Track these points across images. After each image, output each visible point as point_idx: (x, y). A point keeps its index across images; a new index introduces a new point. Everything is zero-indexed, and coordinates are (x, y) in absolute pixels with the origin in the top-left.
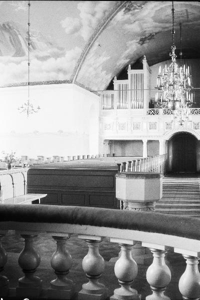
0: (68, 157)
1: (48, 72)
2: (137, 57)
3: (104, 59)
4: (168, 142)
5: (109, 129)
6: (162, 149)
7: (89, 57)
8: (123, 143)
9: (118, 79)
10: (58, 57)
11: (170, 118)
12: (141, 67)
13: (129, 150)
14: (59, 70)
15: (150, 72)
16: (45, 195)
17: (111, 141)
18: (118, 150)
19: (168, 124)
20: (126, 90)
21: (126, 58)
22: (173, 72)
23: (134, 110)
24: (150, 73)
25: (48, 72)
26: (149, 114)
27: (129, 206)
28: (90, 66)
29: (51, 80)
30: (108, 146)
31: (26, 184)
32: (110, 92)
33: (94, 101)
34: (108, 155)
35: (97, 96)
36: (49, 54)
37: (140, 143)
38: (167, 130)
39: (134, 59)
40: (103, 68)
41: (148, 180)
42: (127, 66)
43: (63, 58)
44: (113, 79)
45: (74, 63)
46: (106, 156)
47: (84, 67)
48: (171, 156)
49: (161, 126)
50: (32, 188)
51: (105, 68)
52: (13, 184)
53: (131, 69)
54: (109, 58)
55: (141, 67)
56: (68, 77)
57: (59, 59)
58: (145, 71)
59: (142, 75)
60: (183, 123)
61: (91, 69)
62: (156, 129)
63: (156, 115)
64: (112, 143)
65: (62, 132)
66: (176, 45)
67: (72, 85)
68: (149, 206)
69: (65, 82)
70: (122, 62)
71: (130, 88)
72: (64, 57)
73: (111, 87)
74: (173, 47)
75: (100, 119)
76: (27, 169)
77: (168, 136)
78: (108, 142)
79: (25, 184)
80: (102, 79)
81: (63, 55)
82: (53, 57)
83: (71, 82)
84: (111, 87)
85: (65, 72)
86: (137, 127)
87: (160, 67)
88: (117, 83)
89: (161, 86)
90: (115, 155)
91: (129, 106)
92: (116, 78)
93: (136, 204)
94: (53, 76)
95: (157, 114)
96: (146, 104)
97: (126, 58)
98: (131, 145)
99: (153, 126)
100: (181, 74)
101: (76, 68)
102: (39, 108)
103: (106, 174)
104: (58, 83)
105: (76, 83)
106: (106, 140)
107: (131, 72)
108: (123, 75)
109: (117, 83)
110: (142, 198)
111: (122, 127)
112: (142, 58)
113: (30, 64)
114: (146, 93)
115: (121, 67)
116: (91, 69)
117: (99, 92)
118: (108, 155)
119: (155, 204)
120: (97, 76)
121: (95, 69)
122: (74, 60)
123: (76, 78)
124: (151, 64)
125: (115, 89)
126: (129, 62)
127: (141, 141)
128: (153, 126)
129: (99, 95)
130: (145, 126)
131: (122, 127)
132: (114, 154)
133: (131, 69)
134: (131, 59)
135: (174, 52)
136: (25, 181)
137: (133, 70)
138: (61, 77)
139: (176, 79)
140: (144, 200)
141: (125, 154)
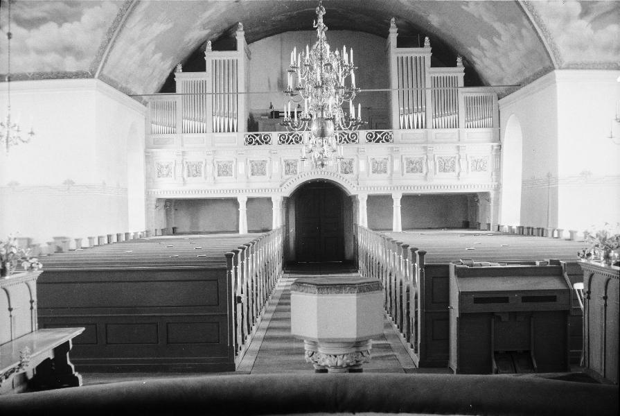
0: (90, 238)
1: (39, 52)
2: (226, 26)
3: (159, 28)
4: (287, 202)
5: (167, 175)
6: (277, 219)
7: (133, 25)
8: (193, 205)
9: (185, 69)
10: (66, 21)
11: (291, 152)
12: (233, 47)
13: (206, 219)
14: (67, 50)
15: (249, 55)
16: (79, 331)
17: (168, 201)
18: (184, 221)
19: (288, 165)
20: (203, 94)
21: (204, 27)
22: (321, 59)
23: (218, 135)
24: (249, 58)
25: (39, 52)
26: (250, 143)
27: (320, 350)
28: (132, 41)
29: (48, 70)
30: (163, 213)
31: (35, 307)
32: (167, 97)
33: (134, 116)
34: (164, 232)
35: (141, 106)
36: (45, 14)
37: (230, 207)
38: (288, 176)
39: (220, 29)
40: (156, 47)
41: (362, 295)
42: (204, 44)
43: (76, 24)
44: (174, 70)
45: (100, 36)
46: (159, 233)
47: (120, 45)
48: (292, 230)
49: (275, 168)
50: (47, 319)
51: (160, 45)
52: (10, 309)
53: (213, 49)
54: (170, 25)
55: (233, 47)
56: (85, 65)
57: (67, 27)
58: (238, 55)
59: (234, 64)
60: (325, 163)
61: (133, 49)
62: (263, 174)
63: (264, 145)
64: (173, 206)
65: (71, 183)
66: (323, 4)
67: (94, 82)
68: (362, 349)
69: (78, 75)
70: (196, 34)
71: (209, 90)
72: (79, 20)
73: (169, 86)
74: (321, 9)
75: (148, 157)
76: (37, 273)
77: (288, 191)
78: (163, 204)
79: (32, 308)
80: (153, 71)
81: (77, 17)
82: (54, 21)
83: (93, 76)
84: (169, 86)
85: (79, 55)
86: (224, 170)
87: (295, 49)
88: (182, 78)
89: (298, 89)
90: (178, 231)
91: (208, 126)
92: (180, 67)
93: (337, 345)
94: (52, 61)
95: (267, 143)
96: (243, 124)
97: (204, 27)
98: (218, 207)
99: (258, 169)
100: (335, 64)
101: (103, 48)
102: (32, 133)
103: (196, 276)
104: (63, 78)
105: (102, 78)
106: (159, 200)
107: (211, 56)
108: (194, 62)
109: (182, 78)
110: (352, 334)
111: (194, 171)
112: (234, 27)
113: (13, 36)
114: (242, 98)
115: (192, 46)
116: (133, 49)
117: (144, 97)
118: (164, 232)
119: (372, 342)
120: (143, 63)
121: (142, 49)
122: (11, 25)
123: (103, 67)
124: (250, 40)
125: (177, 93)
126: (209, 35)
127: (234, 202)
128: (258, 169)
129: (145, 104)
130: (241, 168)
131: (194, 171)
132: (174, 229)
133: (213, 49)
134: (214, 29)
135: (321, 20)
136: (32, 302)
137: (217, 53)
138: (70, 65)
139: (327, 75)
140: (355, 337)
141: (198, 228)
